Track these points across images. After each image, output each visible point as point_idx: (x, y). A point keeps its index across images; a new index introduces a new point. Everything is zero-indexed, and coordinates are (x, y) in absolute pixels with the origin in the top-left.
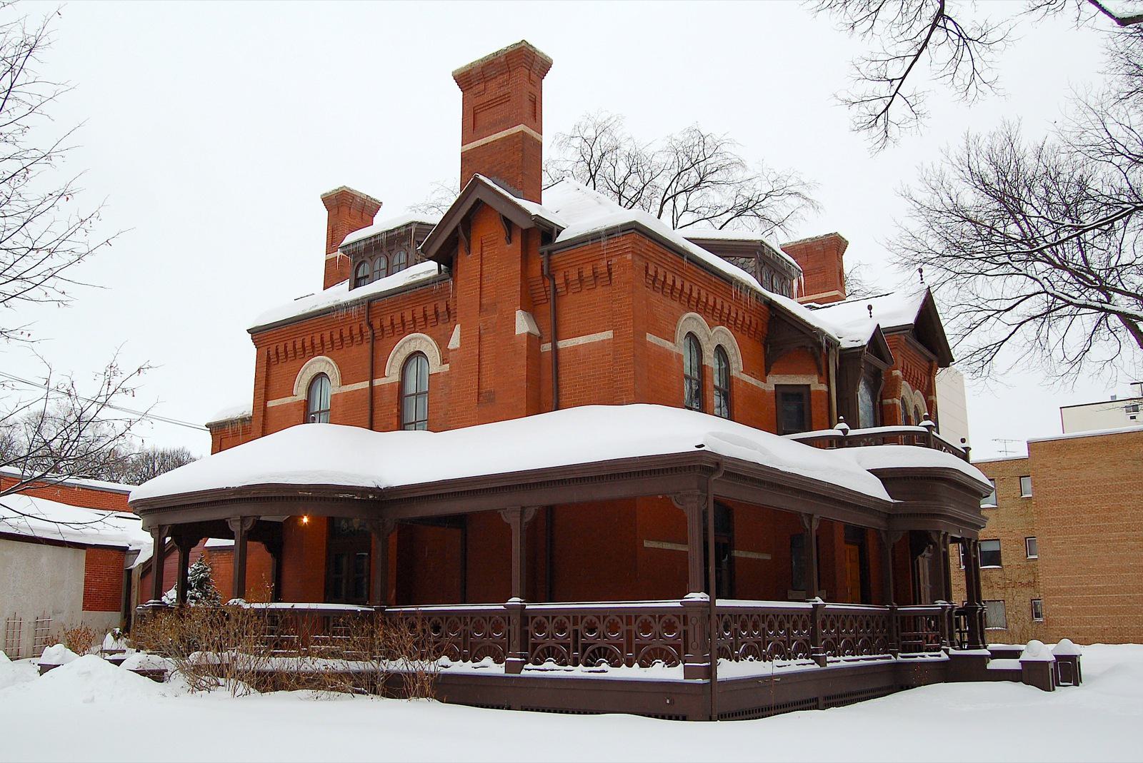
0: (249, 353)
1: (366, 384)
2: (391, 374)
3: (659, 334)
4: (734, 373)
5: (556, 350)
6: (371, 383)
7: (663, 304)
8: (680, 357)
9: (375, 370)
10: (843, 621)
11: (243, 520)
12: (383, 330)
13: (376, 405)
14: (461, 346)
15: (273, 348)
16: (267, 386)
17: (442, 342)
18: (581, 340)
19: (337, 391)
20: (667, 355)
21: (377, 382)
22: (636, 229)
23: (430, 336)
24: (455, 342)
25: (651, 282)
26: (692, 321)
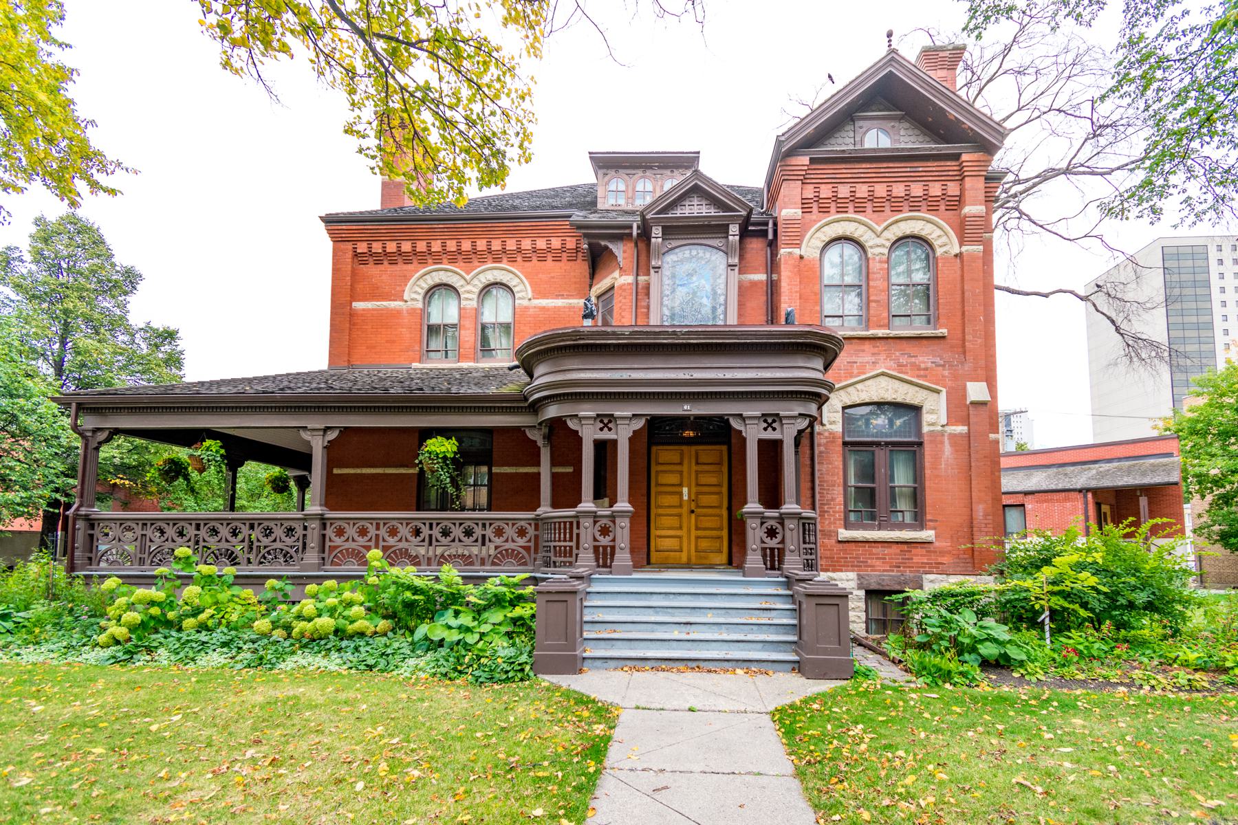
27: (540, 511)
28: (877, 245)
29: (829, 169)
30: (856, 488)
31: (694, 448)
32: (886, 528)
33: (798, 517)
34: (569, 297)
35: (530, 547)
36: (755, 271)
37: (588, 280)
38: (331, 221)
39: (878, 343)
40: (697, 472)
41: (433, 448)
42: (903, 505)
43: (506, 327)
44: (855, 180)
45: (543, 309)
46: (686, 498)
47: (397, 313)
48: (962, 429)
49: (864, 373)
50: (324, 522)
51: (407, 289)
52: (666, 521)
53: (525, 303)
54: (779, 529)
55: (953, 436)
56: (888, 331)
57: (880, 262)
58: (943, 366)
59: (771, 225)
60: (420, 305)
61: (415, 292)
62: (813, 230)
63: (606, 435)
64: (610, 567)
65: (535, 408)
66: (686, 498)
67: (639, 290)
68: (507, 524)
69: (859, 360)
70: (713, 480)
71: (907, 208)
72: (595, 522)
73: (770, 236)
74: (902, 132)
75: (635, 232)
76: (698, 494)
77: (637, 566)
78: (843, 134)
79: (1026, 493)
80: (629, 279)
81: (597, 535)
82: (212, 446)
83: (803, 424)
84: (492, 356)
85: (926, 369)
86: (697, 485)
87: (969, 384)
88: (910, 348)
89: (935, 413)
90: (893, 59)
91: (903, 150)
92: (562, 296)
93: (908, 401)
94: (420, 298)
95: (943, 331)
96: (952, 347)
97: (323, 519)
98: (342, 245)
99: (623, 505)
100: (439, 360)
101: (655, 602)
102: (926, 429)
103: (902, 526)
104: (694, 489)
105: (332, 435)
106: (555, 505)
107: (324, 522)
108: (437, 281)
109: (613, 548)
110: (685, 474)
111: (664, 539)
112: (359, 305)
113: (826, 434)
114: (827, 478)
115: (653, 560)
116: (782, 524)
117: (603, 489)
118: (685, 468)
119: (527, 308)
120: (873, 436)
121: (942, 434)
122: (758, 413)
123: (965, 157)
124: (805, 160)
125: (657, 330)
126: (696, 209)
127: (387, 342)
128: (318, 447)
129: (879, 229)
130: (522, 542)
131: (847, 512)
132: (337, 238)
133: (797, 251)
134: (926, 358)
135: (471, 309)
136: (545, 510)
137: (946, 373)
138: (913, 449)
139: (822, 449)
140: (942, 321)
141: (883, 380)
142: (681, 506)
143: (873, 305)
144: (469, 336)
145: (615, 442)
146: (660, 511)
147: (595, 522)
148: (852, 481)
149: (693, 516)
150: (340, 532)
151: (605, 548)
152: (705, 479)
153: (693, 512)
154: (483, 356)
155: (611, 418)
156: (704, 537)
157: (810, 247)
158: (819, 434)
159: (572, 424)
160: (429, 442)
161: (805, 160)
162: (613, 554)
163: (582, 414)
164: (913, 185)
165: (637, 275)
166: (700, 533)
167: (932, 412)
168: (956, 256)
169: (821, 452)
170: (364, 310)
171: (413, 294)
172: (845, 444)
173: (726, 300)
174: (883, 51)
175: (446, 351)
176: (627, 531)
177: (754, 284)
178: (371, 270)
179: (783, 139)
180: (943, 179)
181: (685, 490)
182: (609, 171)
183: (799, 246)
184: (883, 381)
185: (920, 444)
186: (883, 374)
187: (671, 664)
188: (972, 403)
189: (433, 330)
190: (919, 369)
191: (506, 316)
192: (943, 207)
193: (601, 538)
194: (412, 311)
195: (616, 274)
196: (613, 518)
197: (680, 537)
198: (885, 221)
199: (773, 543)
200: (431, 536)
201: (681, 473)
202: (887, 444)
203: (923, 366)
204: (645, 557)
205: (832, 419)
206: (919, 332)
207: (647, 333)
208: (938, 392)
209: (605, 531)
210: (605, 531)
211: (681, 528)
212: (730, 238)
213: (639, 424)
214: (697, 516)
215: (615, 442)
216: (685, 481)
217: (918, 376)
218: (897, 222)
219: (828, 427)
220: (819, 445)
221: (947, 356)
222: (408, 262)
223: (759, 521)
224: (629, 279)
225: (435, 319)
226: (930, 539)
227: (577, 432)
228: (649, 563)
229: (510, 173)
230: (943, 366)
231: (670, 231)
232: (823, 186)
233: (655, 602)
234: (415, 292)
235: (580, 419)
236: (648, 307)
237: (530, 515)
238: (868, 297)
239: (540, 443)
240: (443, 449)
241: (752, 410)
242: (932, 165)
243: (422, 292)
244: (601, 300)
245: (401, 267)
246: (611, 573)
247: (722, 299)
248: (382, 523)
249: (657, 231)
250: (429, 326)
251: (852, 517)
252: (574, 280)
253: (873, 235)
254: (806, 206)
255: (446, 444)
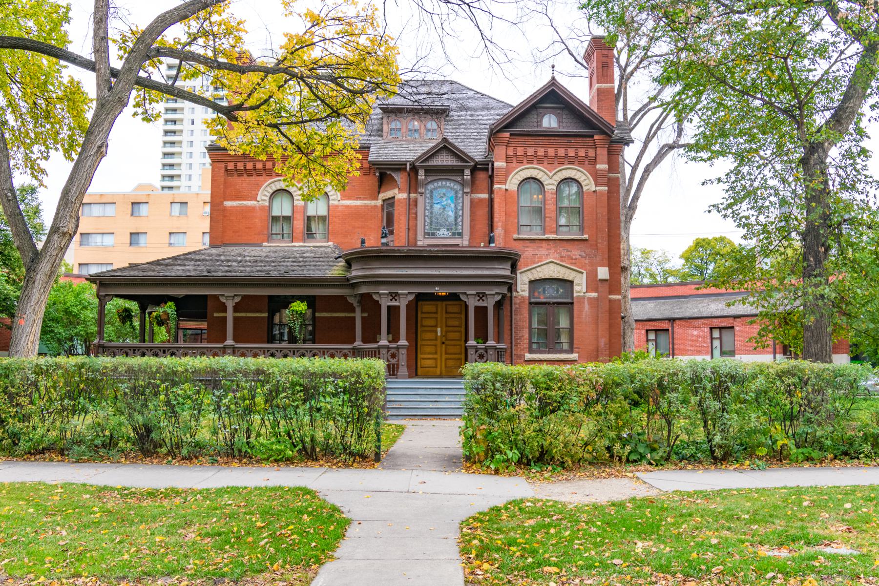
27: (356, 344)
28: (550, 185)
29: (521, 140)
30: (538, 329)
31: (444, 303)
32: (552, 353)
33: (495, 348)
34: (364, 199)
36: (482, 192)
37: (377, 187)
39: (550, 243)
40: (446, 318)
41: (295, 308)
42: (564, 339)
43: (323, 219)
44: (537, 145)
45: (347, 207)
46: (439, 334)
47: (253, 209)
48: (594, 295)
49: (541, 261)
51: (260, 193)
52: (428, 349)
53: (336, 203)
54: (485, 355)
55: (590, 299)
56: (555, 236)
57: (552, 194)
58: (585, 257)
59: (490, 166)
60: (267, 204)
61: (265, 195)
62: (513, 173)
63: (394, 303)
64: (396, 375)
65: (353, 286)
66: (439, 334)
67: (411, 203)
69: (539, 253)
70: (456, 323)
71: (567, 162)
72: (388, 351)
73: (490, 173)
74: (564, 117)
75: (408, 169)
76: (447, 332)
77: (410, 377)
78: (531, 116)
79: (736, 317)
80: (404, 196)
81: (389, 358)
82: (170, 308)
83: (498, 298)
84: (314, 238)
85: (576, 259)
86: (447, 326)
87: (599, 269)
88: (569, 246)
89: (580, 287)
90: (553, 83)
91: (562, 132)
92: (360, 199)
93: (565, 278)
94: (267, 199)
95: (586, 236)
96: (591, 246)
97: (234, 348)
98: (218, 165)
99: (403, 342)
100: (278, 241)
101: (420, 392)
102: (575, 295)
103: (562, 351)
104: (444, 329)
105: (237, 299)
106: (365, 341)
109: (398, 365)
110: (439, 319)
111: (426, 361)
112: (228, 204)
113: (520, 297)
114: (519, 323)
115: (419, 373)
116: (487, 352)
117: (393, 331)
118: (439, 315)
119: (337, 206)
120: (547, 298)
121: (584, 297)
122: (474, 292)
123: (596, 137)
124: (507, 135)
125: (421, 249)
126: (444, 160)
127: (246, 228)
128: (230, 305)
129: (551, 175)
131: (531, 343)
132: (214, 161)
133: (504, 187)
134: (576, 253)
135: (301, 207)
136: (358, 343)
137: (587, 262)
138: (569, 305)
139: (517, 306)
140: (586, 230)
141: (551, 265)
142: (436, 339)
143: (547, 219)
144: (299, 224)
145: (399, 307)
146: (424, 343)
147: (388, 351)
148: (535, 325)
149: (444, 346)
151: (393, 365)
152: (450, 323)
153: (443, 343)
154: (308, 238)
155: (397, 294)
156: (450, 359)
157: (512, 184)
158: (515, 297)
159: (375, 297)
160: (293, 304)
161: (507, 135)
162: (398, 368)
163: (381, 292)
164: (569, 150)
165: (410, 193)
166: (448, 356)
167: (578, 285)
168: (594, 191)
169: (516, 308)
170: (231, 207)
171: (263, 196)
172: (530, 303)
173: (463, 213)
174: (549, 78)
175: (283, 235)
176: (405, 356)
177: (481, 200)
178: (236, 180)
179: (493, 127)
180: (587, 148)
181: (439, 330)
182: (391, 115)
183: (505, 184)
184: (552, 266)
185: (572, 303)
186: (552, 262)
187: (427, 417)
188: (600, 280)
189: (275, 219)
190: (572, 259)
191: (322, 211)
192: (587, 162)
193: (391, 360)
194: (262, 208)
195: (396, 191)
196: (398, 348)
197: (436, 359)
198: (555, 169)
199: (393, 361)
201: (436, 318)
202: (554, 303)
203: (574, 257)
204: (415, 372)
205: (522, 289)
206: (572, 237)
207: (416, 250)
208: (582, 273)
209: (393, 356)
210: (393, 356)
211: (436, 353)
212: (465, 177)
213: (411, 297)
214: (446, 346)
215: (399, 307)
216: (439, 325)
217: (572, 264)
218: (561, 170)
219: (521, 293)
220: (515, 304)
221: (588, 251)
222: (259, 175)
223: (474, 350)
224: (404, 196)
225: (276, 212)
226: (575, 359)
227: (378, 301)
228: (416, 375)
230: (585, 257)
231: (429, 171)
232: (519, 148)
233: (420, 392)
234: (265, 195)
235: (380, 295)
236: (416, 214)
237: (350, 346)
238: (545, 215)
239: (355, 305)
240: (300, 309)
241: (472, 291)
242: (579, 140)
243: (269, 195)
244: (386, 202)
245: (254, 178)
246: (397, 378)
247: (461, 212)
249: (421, 172)
250: (273, 217)
251: (535, 346)
252: (367, 188)
253: (548, 178)
254: (508, 160)
255: (301, 305)
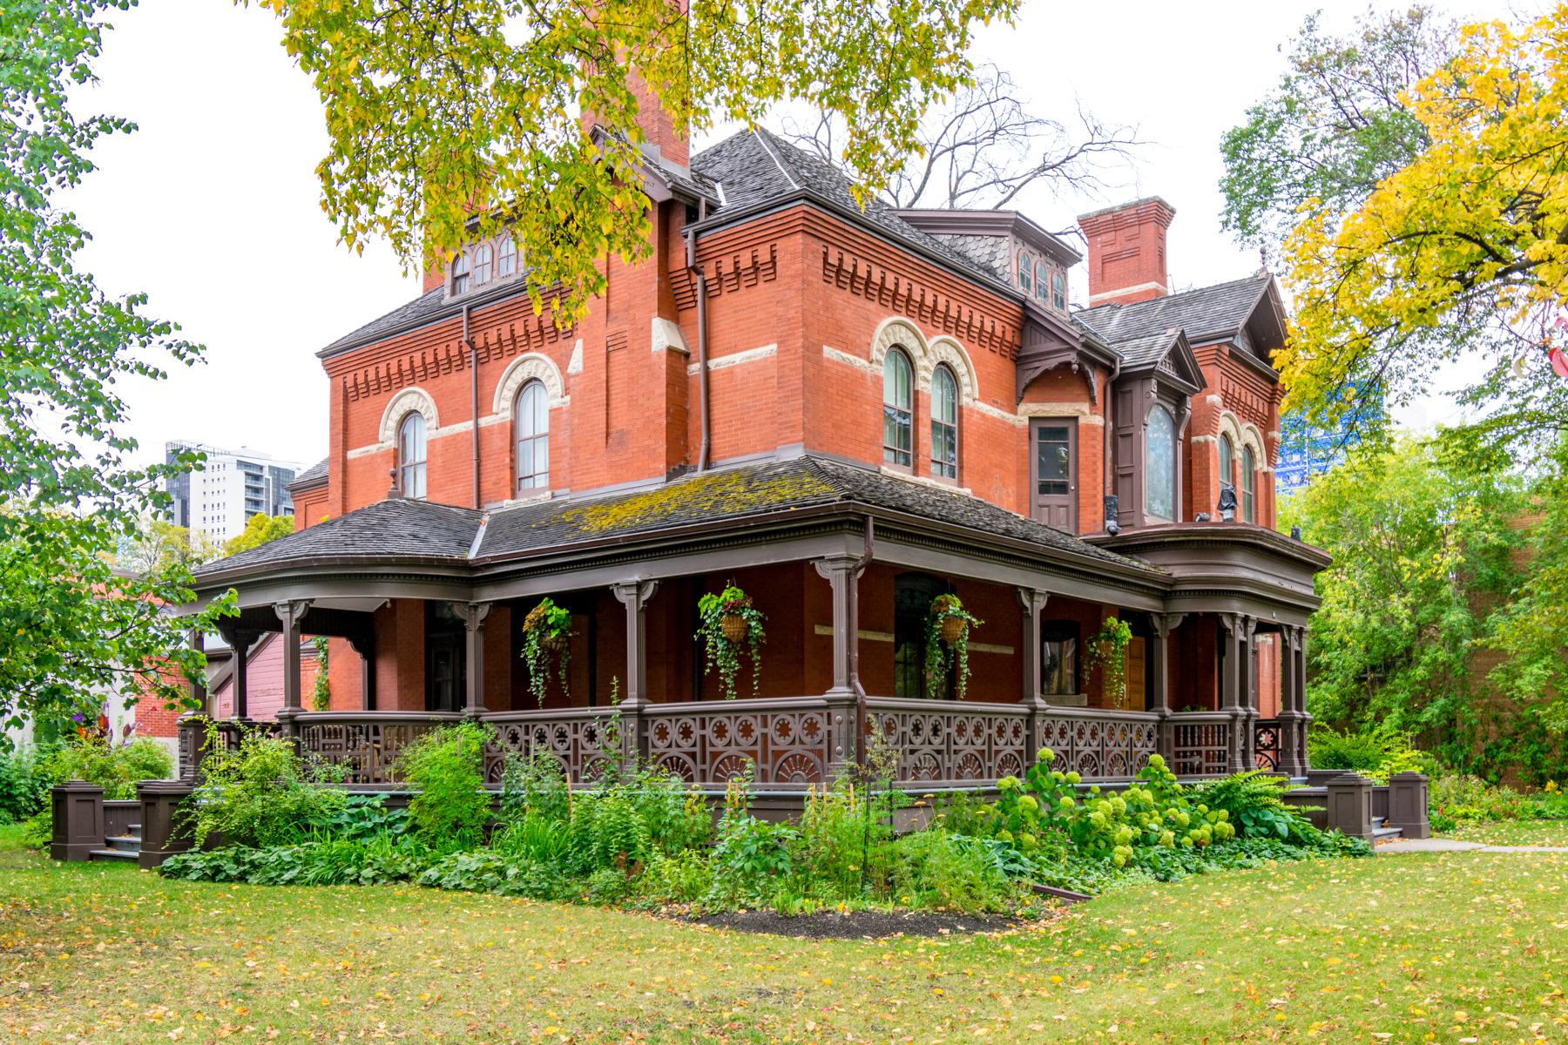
0: (318, 389)
1: (469, 425)
2: (500, 411)
3: (846, 345)
4: (966, 401)
5: (707, 373)
6: (477, 424)
7: (847, 304)
8: (878, 381)
9: (481, 406)
10: (1111, 729)
11: (292, 605)
12: (488, 350)
13: (483, 453)
14: (584, 368)
15: (350, 377)
16: (346, 430)
17: (563, 364)
18: (738, 358)
19: (434, 434)
20: (857, 378)
21: (485, 421)
22: (806, 199)
23: (549, 355)
24: (576, 364)
25: (832, 274)
26: (888, 327)
35: (821, 750)
38: (319, 355)
50: (643, 718)
68: (793, 716)
107: (643, 718)
108: (515, 387)
130: (686, 745)
132: (332, 370)
150: (663, 733)
200: (703, 737)
229: (1230, 129)
248: (769, 715)
